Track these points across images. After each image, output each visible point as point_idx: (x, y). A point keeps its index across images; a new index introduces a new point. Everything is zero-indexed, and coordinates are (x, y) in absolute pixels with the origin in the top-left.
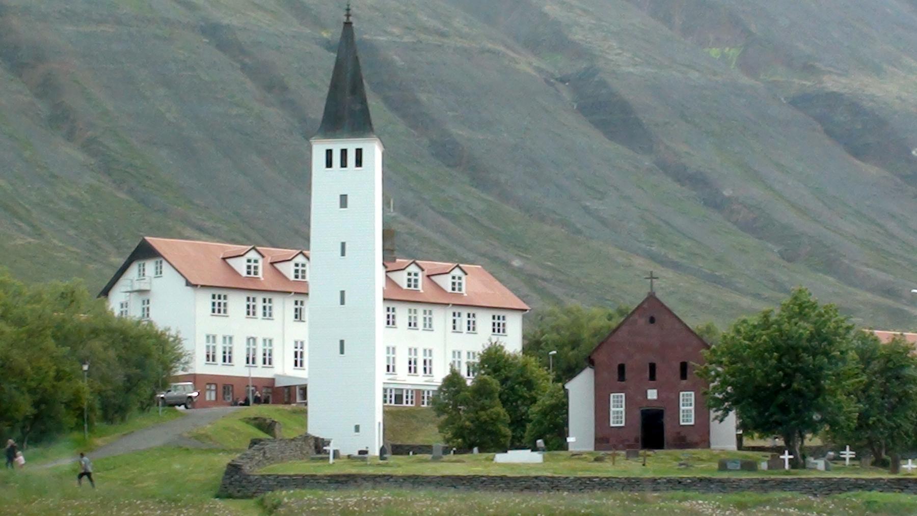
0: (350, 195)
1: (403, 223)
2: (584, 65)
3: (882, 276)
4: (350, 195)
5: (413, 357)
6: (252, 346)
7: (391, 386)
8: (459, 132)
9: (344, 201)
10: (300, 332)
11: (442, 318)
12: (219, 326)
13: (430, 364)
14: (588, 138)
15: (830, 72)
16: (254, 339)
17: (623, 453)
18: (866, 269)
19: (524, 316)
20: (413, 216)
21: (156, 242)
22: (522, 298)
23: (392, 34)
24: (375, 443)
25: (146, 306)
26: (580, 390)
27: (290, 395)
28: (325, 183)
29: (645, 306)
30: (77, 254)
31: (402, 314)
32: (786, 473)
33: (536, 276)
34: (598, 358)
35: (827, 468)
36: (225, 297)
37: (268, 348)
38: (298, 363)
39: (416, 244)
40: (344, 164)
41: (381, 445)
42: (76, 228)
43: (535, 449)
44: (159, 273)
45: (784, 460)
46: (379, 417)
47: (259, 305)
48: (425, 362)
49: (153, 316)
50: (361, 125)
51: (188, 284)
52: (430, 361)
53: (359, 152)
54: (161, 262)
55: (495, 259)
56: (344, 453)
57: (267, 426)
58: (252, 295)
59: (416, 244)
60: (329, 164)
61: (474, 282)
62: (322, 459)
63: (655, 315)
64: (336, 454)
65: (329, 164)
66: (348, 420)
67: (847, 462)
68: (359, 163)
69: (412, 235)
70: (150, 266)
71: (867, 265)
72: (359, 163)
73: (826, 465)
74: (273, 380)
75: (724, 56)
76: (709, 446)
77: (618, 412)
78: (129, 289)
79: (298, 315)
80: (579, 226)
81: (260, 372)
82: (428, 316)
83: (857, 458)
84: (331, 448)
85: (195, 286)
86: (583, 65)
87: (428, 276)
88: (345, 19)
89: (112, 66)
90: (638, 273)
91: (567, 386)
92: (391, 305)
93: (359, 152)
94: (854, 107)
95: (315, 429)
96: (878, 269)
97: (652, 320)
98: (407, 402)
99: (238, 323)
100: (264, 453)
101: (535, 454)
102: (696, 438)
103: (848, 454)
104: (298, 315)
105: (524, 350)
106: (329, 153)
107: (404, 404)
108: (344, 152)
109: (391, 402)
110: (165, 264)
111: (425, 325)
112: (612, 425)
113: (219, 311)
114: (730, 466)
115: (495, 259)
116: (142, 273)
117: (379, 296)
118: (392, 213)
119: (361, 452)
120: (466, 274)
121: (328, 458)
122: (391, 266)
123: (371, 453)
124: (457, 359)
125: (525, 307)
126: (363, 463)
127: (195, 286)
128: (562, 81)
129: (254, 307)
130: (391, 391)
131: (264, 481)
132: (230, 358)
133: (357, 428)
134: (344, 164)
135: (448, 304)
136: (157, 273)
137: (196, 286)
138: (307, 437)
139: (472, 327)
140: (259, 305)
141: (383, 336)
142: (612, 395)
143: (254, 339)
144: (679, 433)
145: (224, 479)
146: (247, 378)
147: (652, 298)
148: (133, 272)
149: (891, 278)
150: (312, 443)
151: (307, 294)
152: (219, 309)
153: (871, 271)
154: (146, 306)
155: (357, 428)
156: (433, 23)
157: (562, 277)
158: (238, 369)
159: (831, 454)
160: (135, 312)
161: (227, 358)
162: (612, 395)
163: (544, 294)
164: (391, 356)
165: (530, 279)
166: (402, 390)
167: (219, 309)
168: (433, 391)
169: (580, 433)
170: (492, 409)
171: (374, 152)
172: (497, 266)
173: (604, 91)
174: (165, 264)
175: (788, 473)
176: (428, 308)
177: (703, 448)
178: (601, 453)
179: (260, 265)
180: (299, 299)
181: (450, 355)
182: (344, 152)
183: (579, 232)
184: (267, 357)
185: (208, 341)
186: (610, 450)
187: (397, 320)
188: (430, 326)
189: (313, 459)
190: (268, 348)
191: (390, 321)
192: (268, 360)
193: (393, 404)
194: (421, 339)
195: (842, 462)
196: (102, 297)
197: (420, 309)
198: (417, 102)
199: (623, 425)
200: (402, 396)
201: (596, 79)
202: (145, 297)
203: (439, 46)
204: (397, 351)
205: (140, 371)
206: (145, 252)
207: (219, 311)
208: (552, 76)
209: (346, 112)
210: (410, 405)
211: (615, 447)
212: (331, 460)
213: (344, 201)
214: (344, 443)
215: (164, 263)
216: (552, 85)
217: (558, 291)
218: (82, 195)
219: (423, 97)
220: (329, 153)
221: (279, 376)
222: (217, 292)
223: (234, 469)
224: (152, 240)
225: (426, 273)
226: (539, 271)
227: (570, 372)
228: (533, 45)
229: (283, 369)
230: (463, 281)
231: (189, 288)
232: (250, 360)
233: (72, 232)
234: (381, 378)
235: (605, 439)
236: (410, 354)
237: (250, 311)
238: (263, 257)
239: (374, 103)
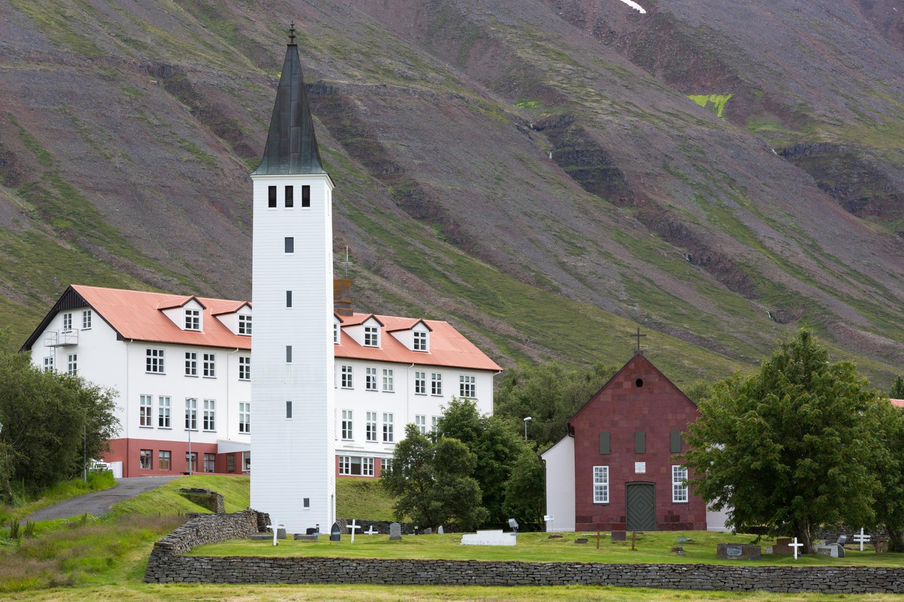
0: (295, 235)
1: (366, 278)
2: (560, 113)
3: (882, 340)
4: (295, 235)
5: (372, 422)
6: (191, 409)
7: (347, 454)
8: (430, 183)
9: (289, 244)
10: (244, 391)
11: (404, 379)
12: (155, 385)
13: (350, 427)
14: (566, 196)
15: (823, 122)
16: (194, 401)
17: (609, 534)
18: (863, 333)
19: (496, 379)
20: (377, 272)
21: (84, 291)
22: (495, 359)
23: (351, 77)
24: (326, 521)
25: (73, 362)
26: (559, 460)
27: (231, 463)
28: (268, 224)
29: (632, 366)
30: (16, 307)
31: (359, 373)
32: (796, 562)
33: (510, 337)
34: (580, 424)
35: (841, 555)
36: (161, 353)
37: (209, 410)
38: (244, 427)
39: (381, 300)
40: (289, 203)
41: (335, 521)
42: (13, 279)
43: (507, 529)
44: (87, 324)
45: (793, 547)
46: (332, 490)
47: (200, 362)
48: (385, 428)
49: (80, 374)
50: (307, 157)
51: (120, 337)
52: (350, 423)
53: (306, 190)
54: (90, 313)
55: (466, 317)
56: (290, 531)
57: (209, 500)
58: (191, 351)
59: (381, 300)
60: (272, 203)
61: (444, 340)
62: (264, 538)
63: (643, 377)
64: (282, 534)
65: (272, 203)
66: (295, 492)
67: (862, 547)
68: (306, 202)
69: (376, 291)
70: (77, 317)
71: (864, 328)
72: (306, 202)
73: (840, 550)
74: (216, 445)
75: (710, 105)
76: (705, 528)
77: (601, 488)
78: (54, 343)
79: (244, 373)
80: (555, 283)
81: (201, 437)
82: (388, 376)
83: (874, 542)
84: (275, 526)
85: (127, 340)
86: (559, 111)
87: (388, 332)
88: (289, 41)
89: (52, 108)
90: (619, 334)
91: (544, 457)
92: (347, 364)
93: (306, 190)
94: (851, 159)
95: (256, 505)
96: (876, 332)
97: (639, 383)
98: (365, 472)
99: (175, 384)
100: (197, 531)
101: (508, 534)
102: (691, 518)
103: (862, 537)
104: (244, 373)
105: (496, 413)
106: (272, 190)
107: (362, 474)
108: (289, 190)
109: (347, 471)
110: (94, 315)
111: (385, 386)
112: (595, 502)
113: (155, 369)
114: (729, 551)
115: (466, 317)
116: (68, 325)
117: (331, 353)
118: (347, 263)
119: (310, 531)
120: (430, 330)
121: (272, 538)
122: (347, 320)
123: (322, 531)
124: (245, 413)
125: (497, 367)
126: (311, 544)
127: (127, 340)
128: (538, 129)
129: (194, 364)
130: (347, 458)
131: (197, 564)
132: (212, 423)
133: (307, 502)
134: (289, 203)
135: (411, 364)
136: (85, 325)
137: (130, 340)
138: (248, 513)
139: (436, 389)
140: (200, 362)
141: (336, 401)
142: (594, 467)
143: (194, 401)
144: (670, 512)
145: (151, 561)
146: (187, 443)
147: (639, 359)
148: (58, 322)
149: (889, 342)
150: (254, 519)
151: (250, 350)
152: (154, 366)
153: (870, 335)
154: (73, 362)
155: (307, 502)
156: (399, 67)
157: (537, 338)
158: (177, 433)
159: (844, 537)
160: (61, 367)
161: (164, 422)
162: (594, 467)
163: (516, 353)
164: (245, 413)
165: (504, 340)
166: (360, 458)
167: (154, 366)
168: (389, 461)
169: (559, 511)
170: (458, 480)
171: (322, 189)
172: (469, 326)
173: (581, 141)
174: (94, 315)
175: (797, 562)
176: (388, 367)
177: (699, 529)
178: (584, 534)
179: (201, 317)
180: (245, 355)
181: (340, 414)
182: (289, 190)
183: (556, 290)
184: (191, 419)
185: (242, 409)
186: (593, 530)
187: (354, 381)
188: (391, 387)
189: (254, 538)
190: (209, 410)
191: (346, 382)
192: (209, 424)
193: (350, 474)
194: (379, 402)
195: (856, 546)
196: (25, 353)
197: (380, 368)
198: (381, 149)
199: (607, 502)
200: (359, 465)
201: (573, 127)
202: (72, 352)
203: (404, 90)
204: (394, 417)
205: (57, 436)
206: (71, 302)
207: (155, 369)
208: (526, 123)
209: (289, 145)
210: (368, 475)
211: (599, 527)
212: (275, 541)
213: (289, 244)
214: (288, 518)
215: (93, 313)
216: (525, 132)
217: (534, 353)
218: (20, 244)
219: (387, 144)
220: (272, 190)
221: (222, 441)
222: (152, 348)
223: (162, 549)
224: (81, 290)
225: (386, 328)
226: (513, 331)
227: (554, 439)
228: (506, 88)
229: (226, 436)
230: (427, 338)
231: (121, 342)
232: (190, 422)
233: (10, 284)
234: (335, 444)
235: (587, 518)
236: (369, 419)
237: (190, 369)
238: (204, 308)
239: (322, 134)
